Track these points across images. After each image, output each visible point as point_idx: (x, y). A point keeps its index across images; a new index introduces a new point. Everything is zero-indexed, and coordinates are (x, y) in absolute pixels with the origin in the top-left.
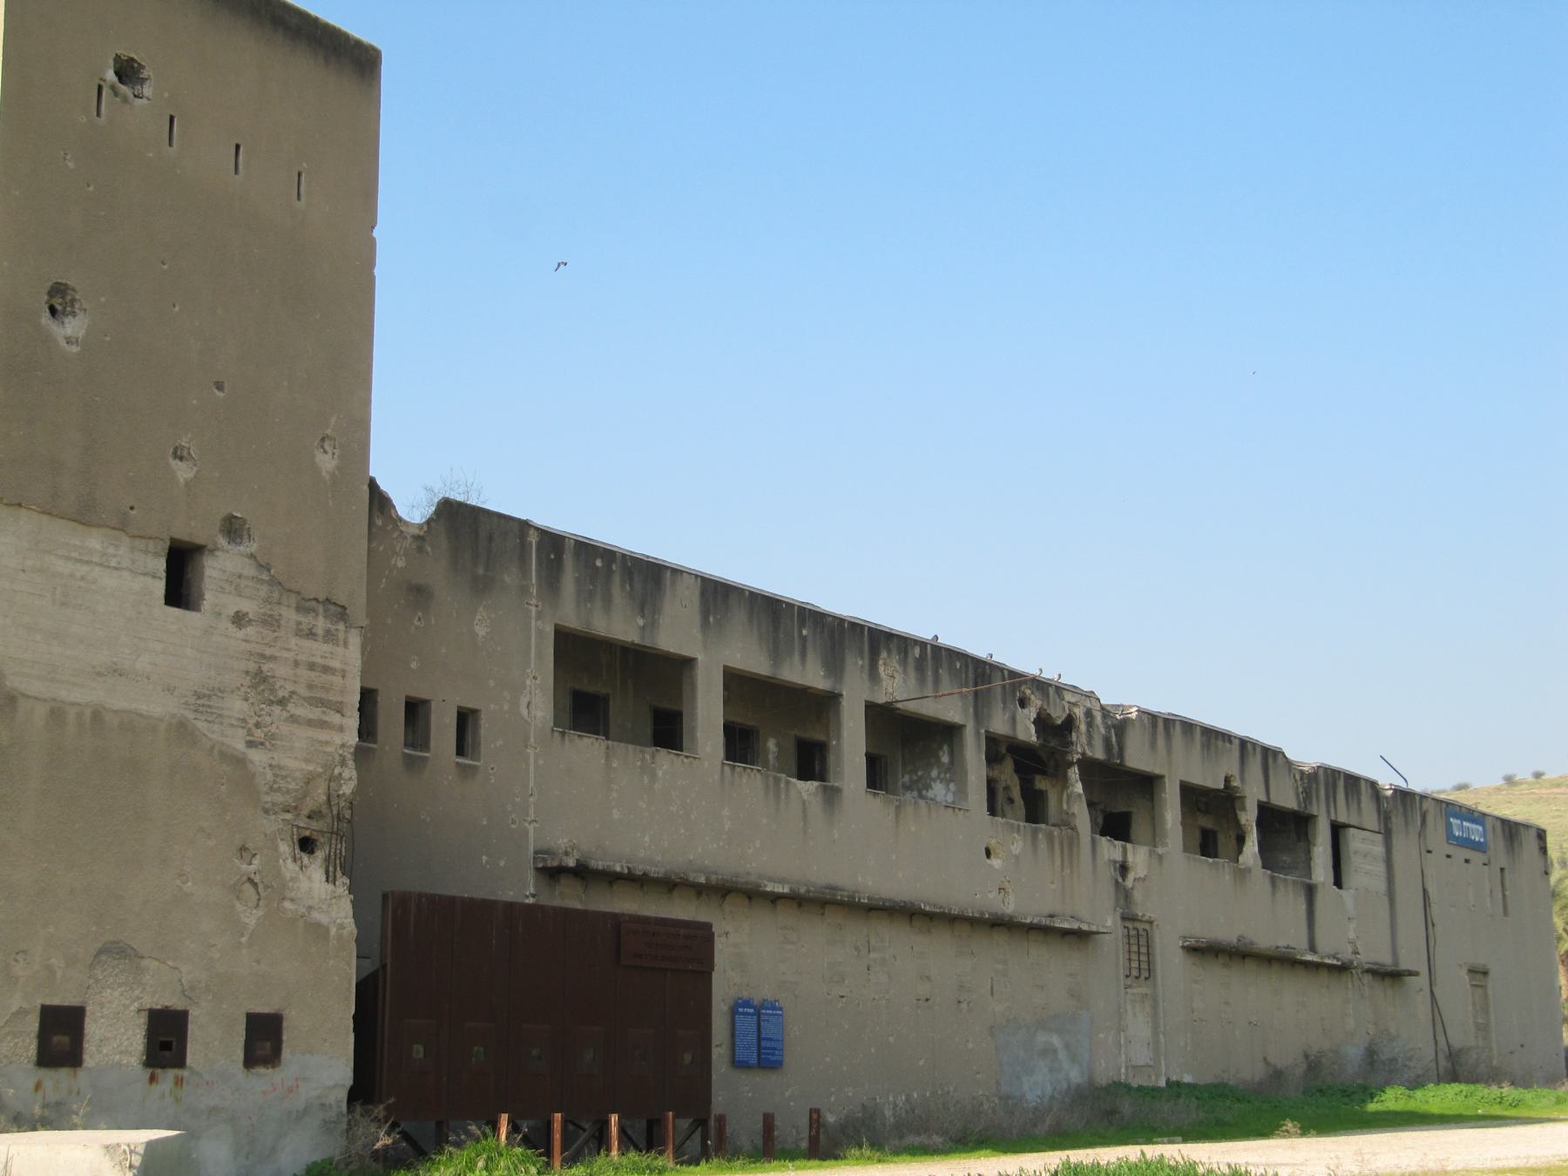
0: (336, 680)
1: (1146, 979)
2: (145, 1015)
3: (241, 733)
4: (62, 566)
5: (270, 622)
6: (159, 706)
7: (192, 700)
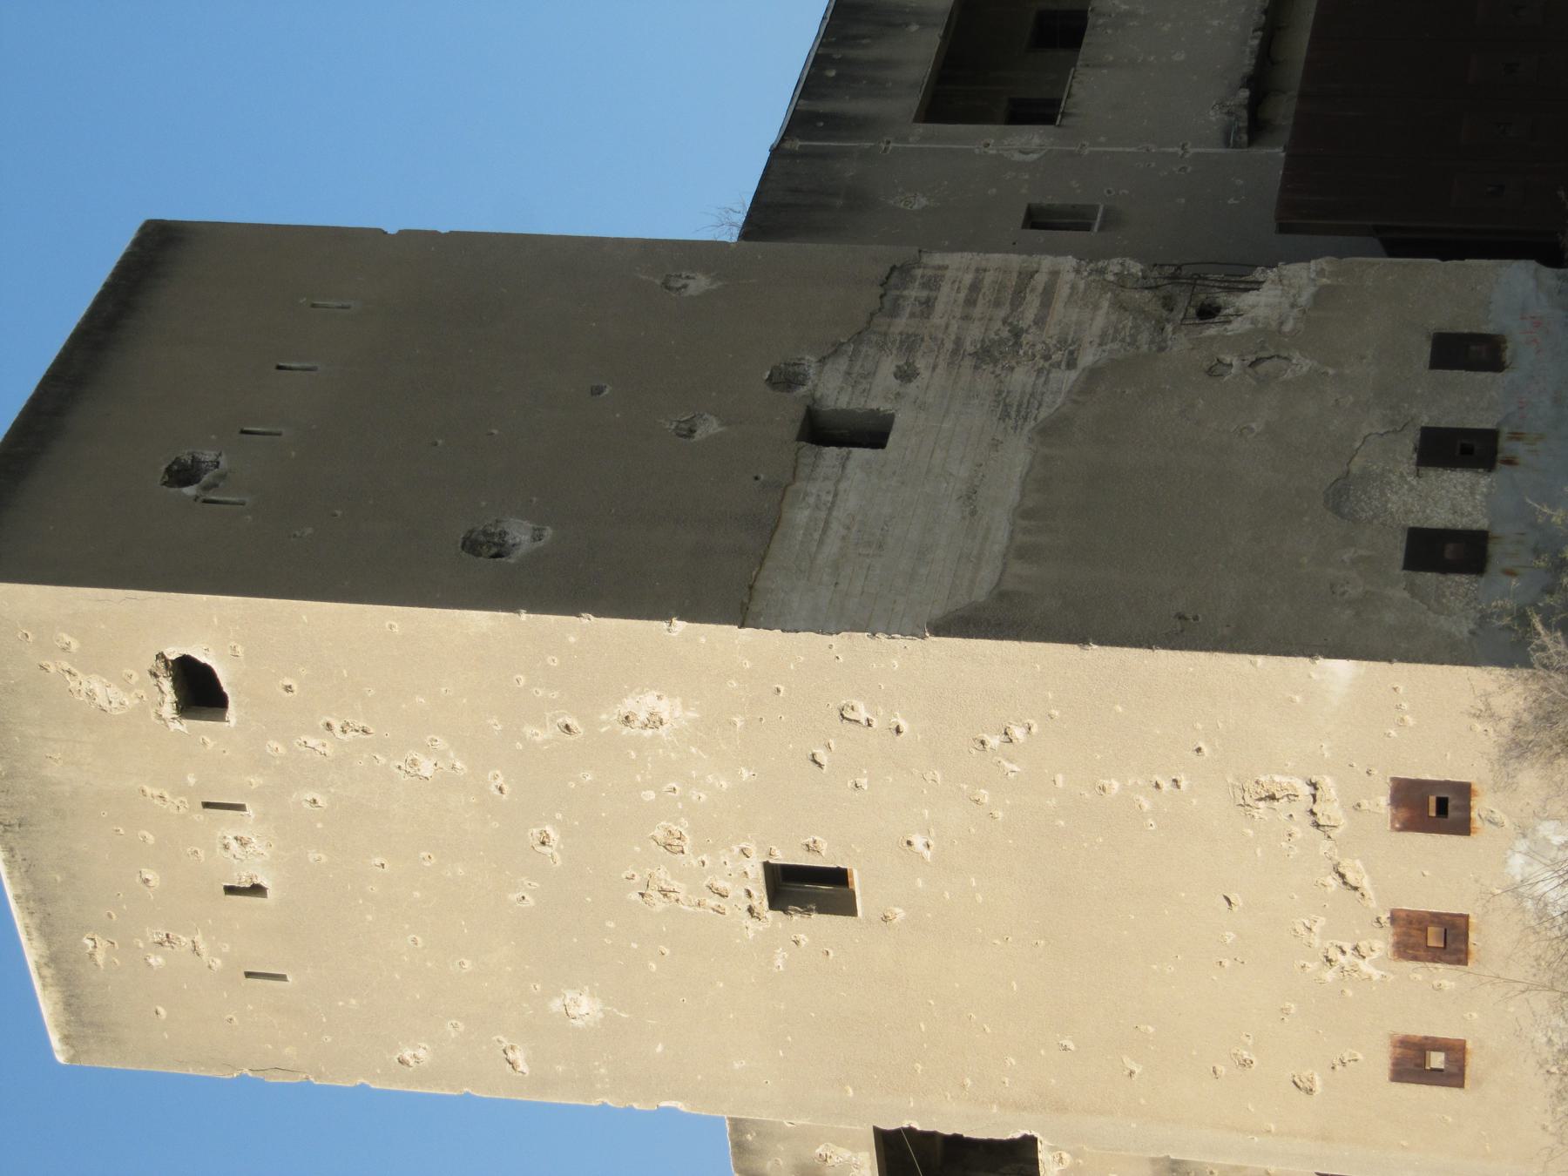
0: (989, 278)
2: (1423, 470)
3: (1055, 374)
4: (832, 547)
5: (909, 344)
6: (1018, 456)
7: (1011, 423)
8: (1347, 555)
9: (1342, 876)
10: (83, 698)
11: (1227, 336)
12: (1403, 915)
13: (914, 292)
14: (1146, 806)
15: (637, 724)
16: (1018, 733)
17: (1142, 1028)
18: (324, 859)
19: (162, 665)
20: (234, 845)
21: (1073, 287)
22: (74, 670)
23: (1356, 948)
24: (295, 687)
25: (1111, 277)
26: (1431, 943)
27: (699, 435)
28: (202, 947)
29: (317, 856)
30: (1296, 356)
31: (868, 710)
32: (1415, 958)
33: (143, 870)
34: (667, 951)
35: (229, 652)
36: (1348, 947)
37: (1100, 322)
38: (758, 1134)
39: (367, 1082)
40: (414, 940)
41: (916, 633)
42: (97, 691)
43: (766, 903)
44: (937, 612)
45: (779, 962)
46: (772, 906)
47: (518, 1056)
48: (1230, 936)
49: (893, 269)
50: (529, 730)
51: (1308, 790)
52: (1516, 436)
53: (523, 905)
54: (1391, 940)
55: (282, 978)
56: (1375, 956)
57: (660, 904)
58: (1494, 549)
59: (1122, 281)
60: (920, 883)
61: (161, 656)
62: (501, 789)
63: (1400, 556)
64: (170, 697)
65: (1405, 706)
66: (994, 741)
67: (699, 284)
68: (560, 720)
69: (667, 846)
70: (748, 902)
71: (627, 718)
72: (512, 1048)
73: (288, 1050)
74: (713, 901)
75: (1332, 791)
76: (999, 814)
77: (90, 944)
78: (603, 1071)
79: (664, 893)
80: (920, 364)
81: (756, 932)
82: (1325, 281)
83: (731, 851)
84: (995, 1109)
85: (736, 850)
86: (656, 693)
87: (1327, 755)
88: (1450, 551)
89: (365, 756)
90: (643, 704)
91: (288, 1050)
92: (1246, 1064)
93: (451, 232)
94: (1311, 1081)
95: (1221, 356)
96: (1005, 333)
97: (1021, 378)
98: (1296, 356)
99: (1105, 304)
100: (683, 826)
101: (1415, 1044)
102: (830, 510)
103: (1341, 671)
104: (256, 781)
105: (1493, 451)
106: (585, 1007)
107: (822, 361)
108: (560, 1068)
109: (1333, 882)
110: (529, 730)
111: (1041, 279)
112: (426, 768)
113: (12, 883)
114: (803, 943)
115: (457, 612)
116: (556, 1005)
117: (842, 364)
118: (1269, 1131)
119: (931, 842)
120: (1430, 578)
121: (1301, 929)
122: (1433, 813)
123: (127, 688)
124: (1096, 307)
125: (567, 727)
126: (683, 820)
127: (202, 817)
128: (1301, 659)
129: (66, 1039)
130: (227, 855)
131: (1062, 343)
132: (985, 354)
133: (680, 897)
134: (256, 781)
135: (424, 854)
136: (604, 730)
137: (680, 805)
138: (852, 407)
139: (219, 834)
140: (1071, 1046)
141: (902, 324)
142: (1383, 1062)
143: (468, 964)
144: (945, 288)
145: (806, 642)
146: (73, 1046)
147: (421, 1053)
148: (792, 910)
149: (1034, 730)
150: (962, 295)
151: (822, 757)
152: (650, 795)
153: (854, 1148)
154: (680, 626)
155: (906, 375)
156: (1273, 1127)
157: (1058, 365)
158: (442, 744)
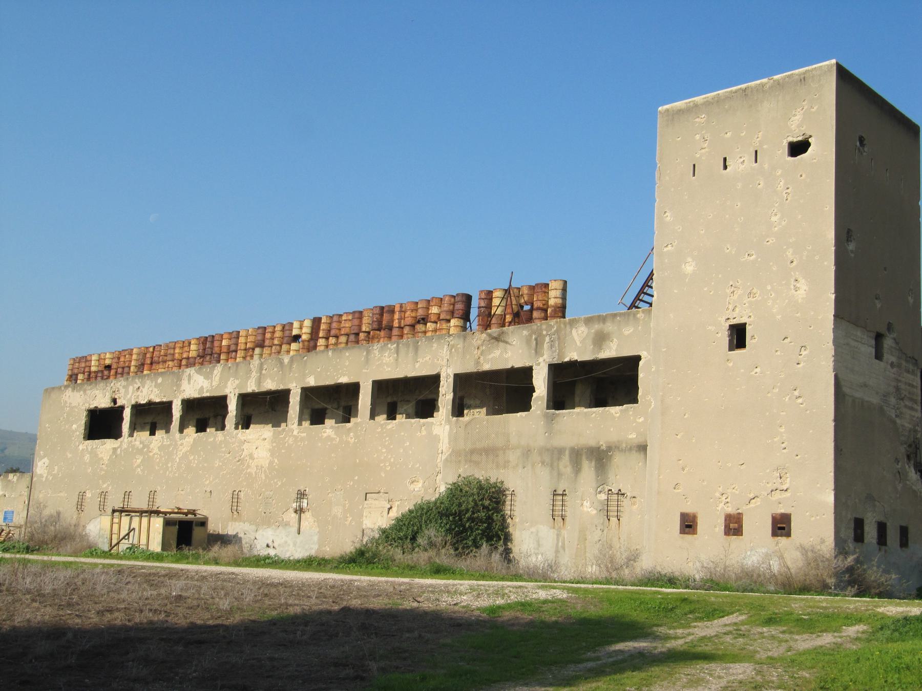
0: (915, 390)
1: (235, 491)
2: (877, 523)
3: (894, 411)
4: (853, 343)
5: (899, 366)
6: (875, 400)
7: (882, 397)
8: (857, 500)
9: (754, 499)
10: (793, 113)
11: (179, 461)
12: (741, 516)
13: (911, 367)
14: (775, 440)
15: (795, 284)
16: (800, 401)
17: (694, 438)
18: (738, 188)
19: (807, 137)
20: (742, 160)
21: (914, 416)
22: (804, 110)
23: (727, 502)
24: (801, 178)
25: (916, 428)
26: (731, 525)
27: (877, 301)
28: (703, 151)
29: (740, 186)
30: (901, 485)
31: (805, 355)
32: (726, 520)
33: (731, 133)
34: (711, 293)
35: (814, 157)
36: (727, 500)
37: (907, 425)
38: (620, 321)
39: (657, 202)
40: (710, 216)
41: (835, 369)
42: (796, 117)
43: (731, 323)
44: (839, 376)
45: (710, 328)
46: (730, 326)
47: (669, 247)
48: (730, 465)
49: (916, 360)
50: (791, 250)
51: (785, 488)
52: (886, 551)
53: (725, 249)
54: (732, 513)
55: (694, 175)
56: (726, 508)
57: (729, 291)
58: (860, 544)
59: (916, 431)
60: (742, 371)
61: (811, 136)
62: (768, 242)
63: (858, 516)
64: (795, 140)
65: (818, 517)
66: (796, 393)
67: (911, 300)
68: (795, 260)
69: (750, 293)
70: (732, 318)
71: (797, 280)
72: (672, 246)
73: (667, 178)
74: (731, 307)
75: (785, 496)
76: (769, 395)
77: (703, 116)
78: (666, 274)
79: (733, 292)
80: (895, 369)
81: (721, 321)
82: (919, 493)
83: (750, 313)
84: (661, 394)
85: (751, 314)
86: (807, 289)
87: (798, 494)
88: (859, 531)
89: (778, 200)
90: (803, 286)
91: (667, 178)
92: (683, 469)
93: (920, 223)
94: (678, 489)
95: (900, 462)
96: (903, 396)
97: (893, 400)
98: (901, 485)
99: (910, 426)
100: (758, 298)
101: (694, 520)
102: (860, 342)
103: (830, 498)
104: (766, 166)
105: (882, 545)
106: (689, 268)
107: (894, 339)
108: (666, 261)
109: (752, 496)
110: (791, 250)
111: (915, 406)
112: (774, 219)
113: (723, 93)
114: (717, 335)
115: (833, 228)
116: (689, 259)
117: (894, 345)
118: (659, 476)
119: (757, 374)
120: (852, 525)
121: (734, 486)
122: (779, 525)
123: (799, 126)
124: (909, 423)
125: (792, 262)
126: (760, 298)
127: (751, 150)
128: (833, 486)
129: (667, 110)
130: (738, 158)
131: (901, 413)
132: (898, 389)
133: (731, 297)
134: (766, 166)
135: (742, 218)
136: (792, 273)
137: (766, 297)
138: (884, 349)
139: (745, 155)
140: (685, 417)
141: (904, 363)
142: (688, 510)
143: (703, 232)
144: (913, 377)
145: (830, 336)
146: (664, 112)
147: (668, 218)
148: (479, 319)
149: (801, 405)
150: (911, 382)
151: (786, 341)
152: (769, 288)
153: (616, 350)
154: (833, 296)
155: (892, 365)
156: (661, 477)
157: (896, 412)
158: (784, 223)
